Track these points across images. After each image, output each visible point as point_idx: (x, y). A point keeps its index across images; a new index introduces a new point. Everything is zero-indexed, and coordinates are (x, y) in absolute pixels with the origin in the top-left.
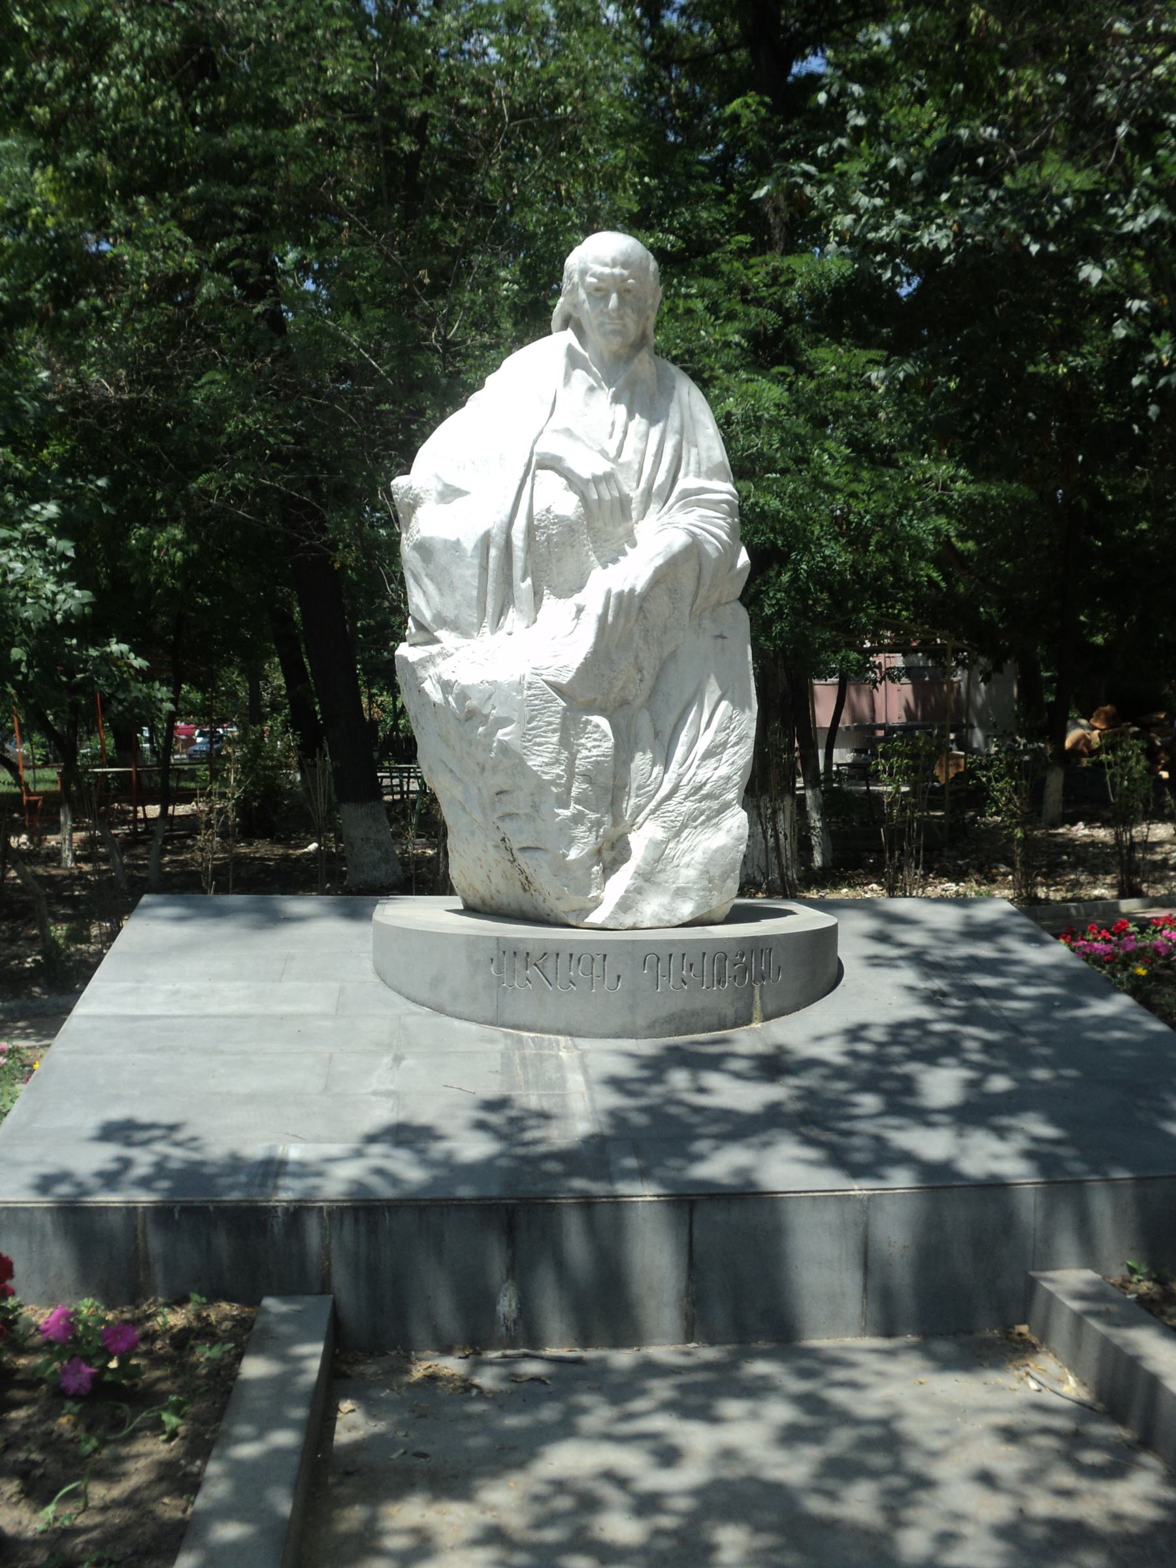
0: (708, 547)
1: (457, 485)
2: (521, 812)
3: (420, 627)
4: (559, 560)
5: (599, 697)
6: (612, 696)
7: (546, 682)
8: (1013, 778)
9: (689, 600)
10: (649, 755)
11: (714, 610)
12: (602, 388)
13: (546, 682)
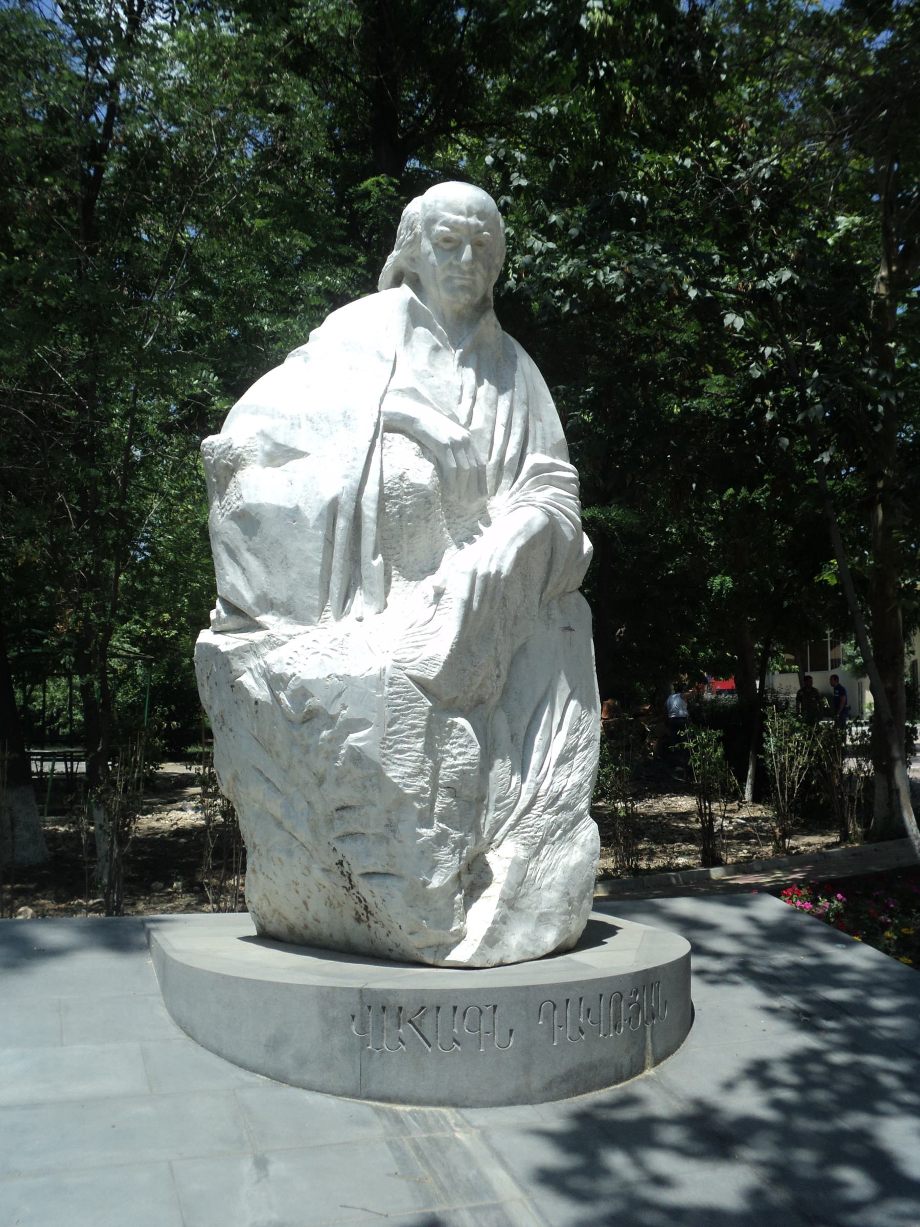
0: (564, 528)
1: (292, 445)
2: (369, 831)
3: (233, 610)
4: (411, 536)
5: (461, 695)
7: (410, 677)
8: (617, 764)
9: (538, 588)
11: (560, 600)
12: (448, 349)
13: (410, 677)
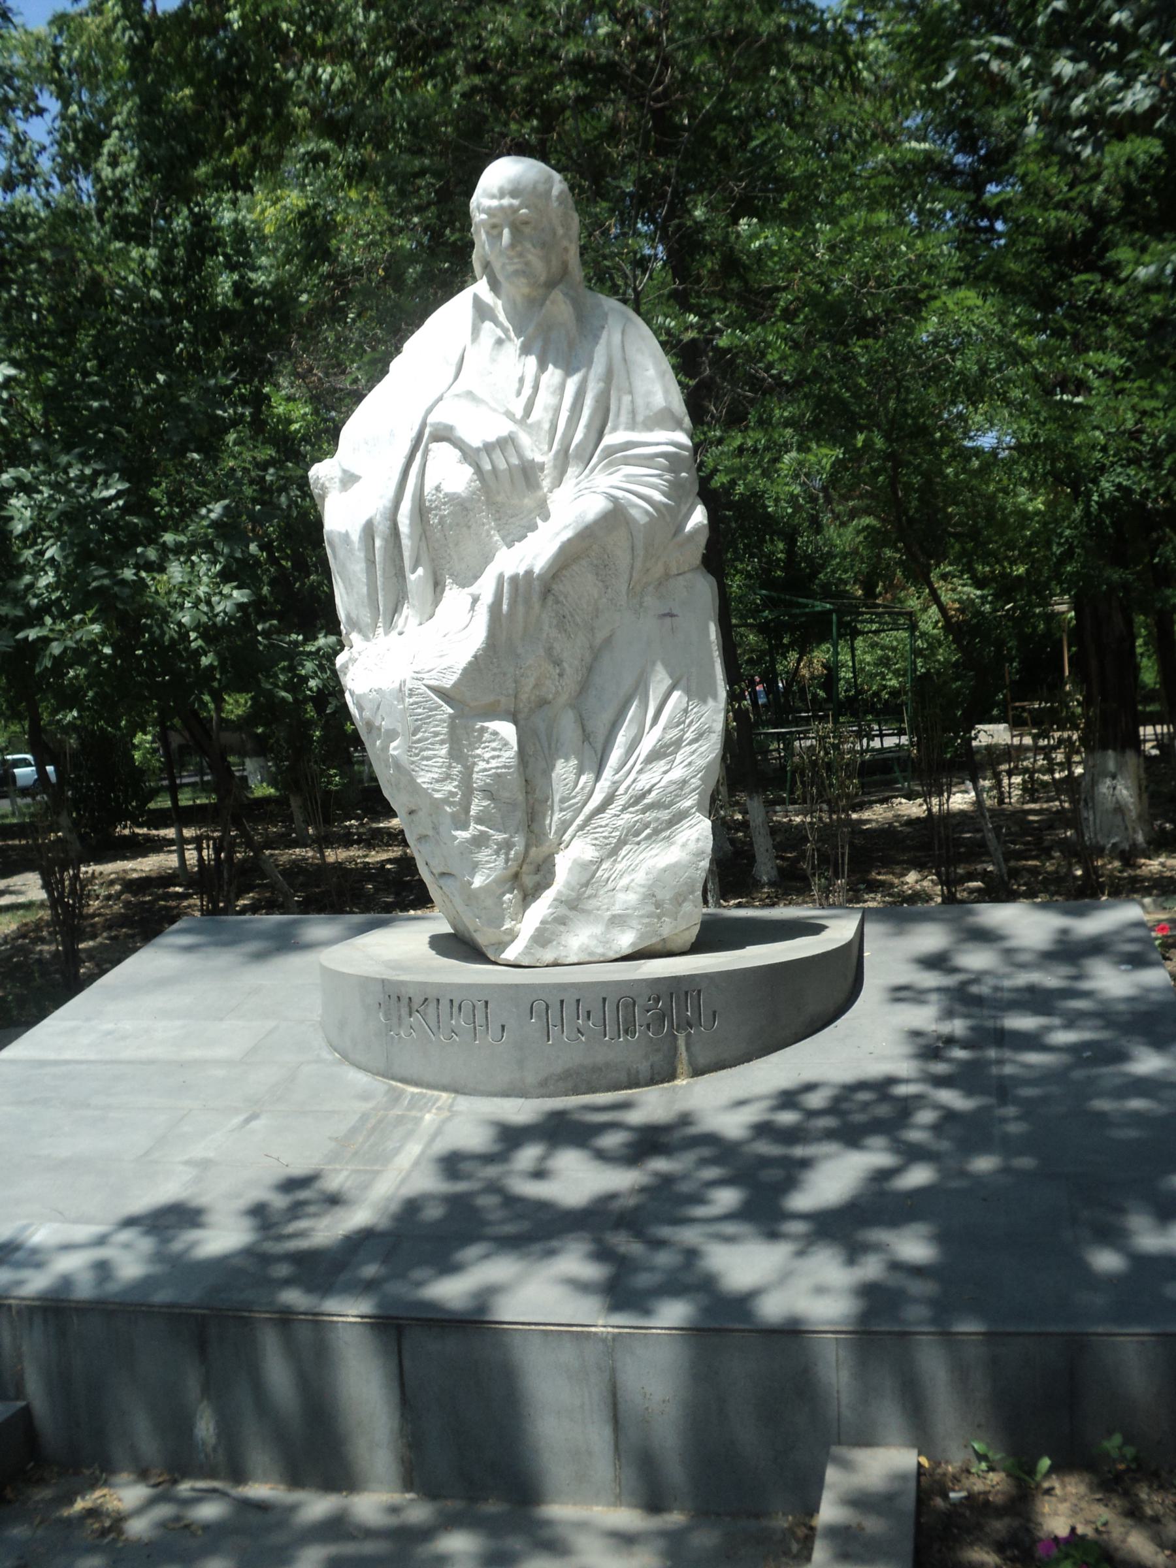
6: (524, 697)
7: (429, 687)
9: (626, 576)
10: (574, 762)
13: (429, 687)
